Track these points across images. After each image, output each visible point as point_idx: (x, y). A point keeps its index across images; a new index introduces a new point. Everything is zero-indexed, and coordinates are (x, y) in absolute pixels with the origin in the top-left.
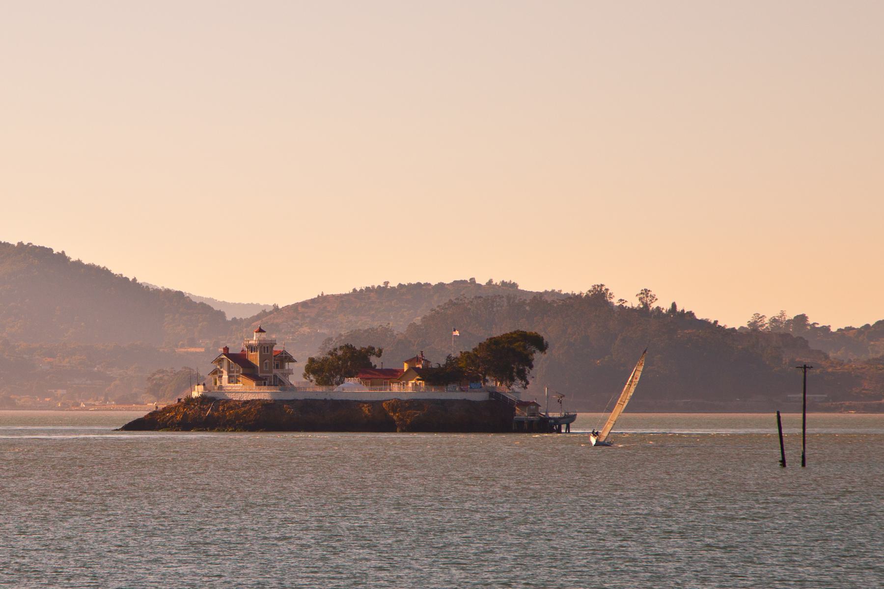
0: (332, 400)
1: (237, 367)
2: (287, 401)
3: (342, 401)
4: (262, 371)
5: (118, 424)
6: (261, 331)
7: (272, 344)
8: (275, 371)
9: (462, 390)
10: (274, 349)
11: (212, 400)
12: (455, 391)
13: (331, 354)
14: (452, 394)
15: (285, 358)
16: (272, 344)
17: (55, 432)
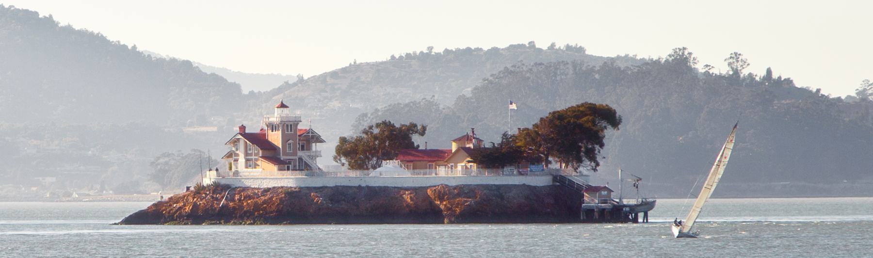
0: (368, 187)
1: (255, 150)
2: (315, 188)
3: (380, 187)
4: (285, 154)
5: (117, 218)
6: (283, 106)
7: (296, 123)
8: (300, 153)
9: (520, 174)
10: (299, 127)
11: (227, 187)
12: (513, 175)
13: (365, 132)
14: (508, 178)
15: (309, 139)
16: (296, 123)
17: (43, 227)
